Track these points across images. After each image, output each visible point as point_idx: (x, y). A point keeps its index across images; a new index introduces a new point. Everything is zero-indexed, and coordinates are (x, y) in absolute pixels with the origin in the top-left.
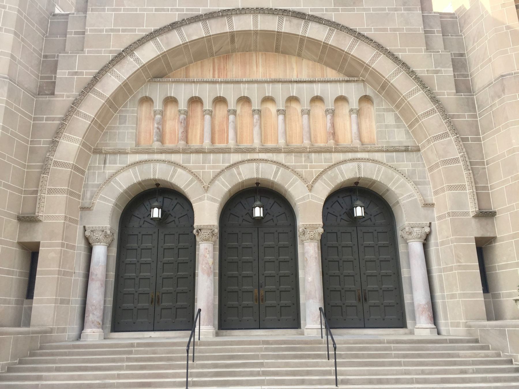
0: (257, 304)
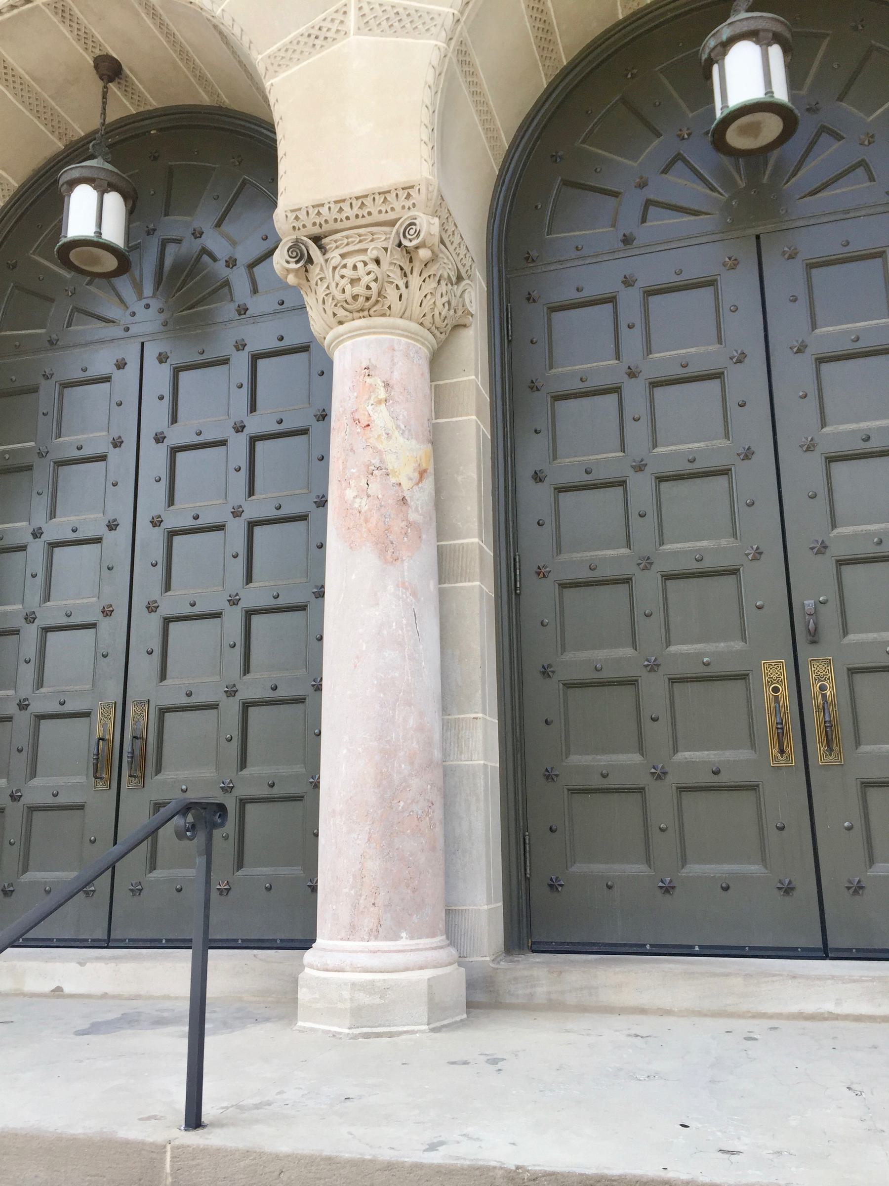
0: (795, 761)
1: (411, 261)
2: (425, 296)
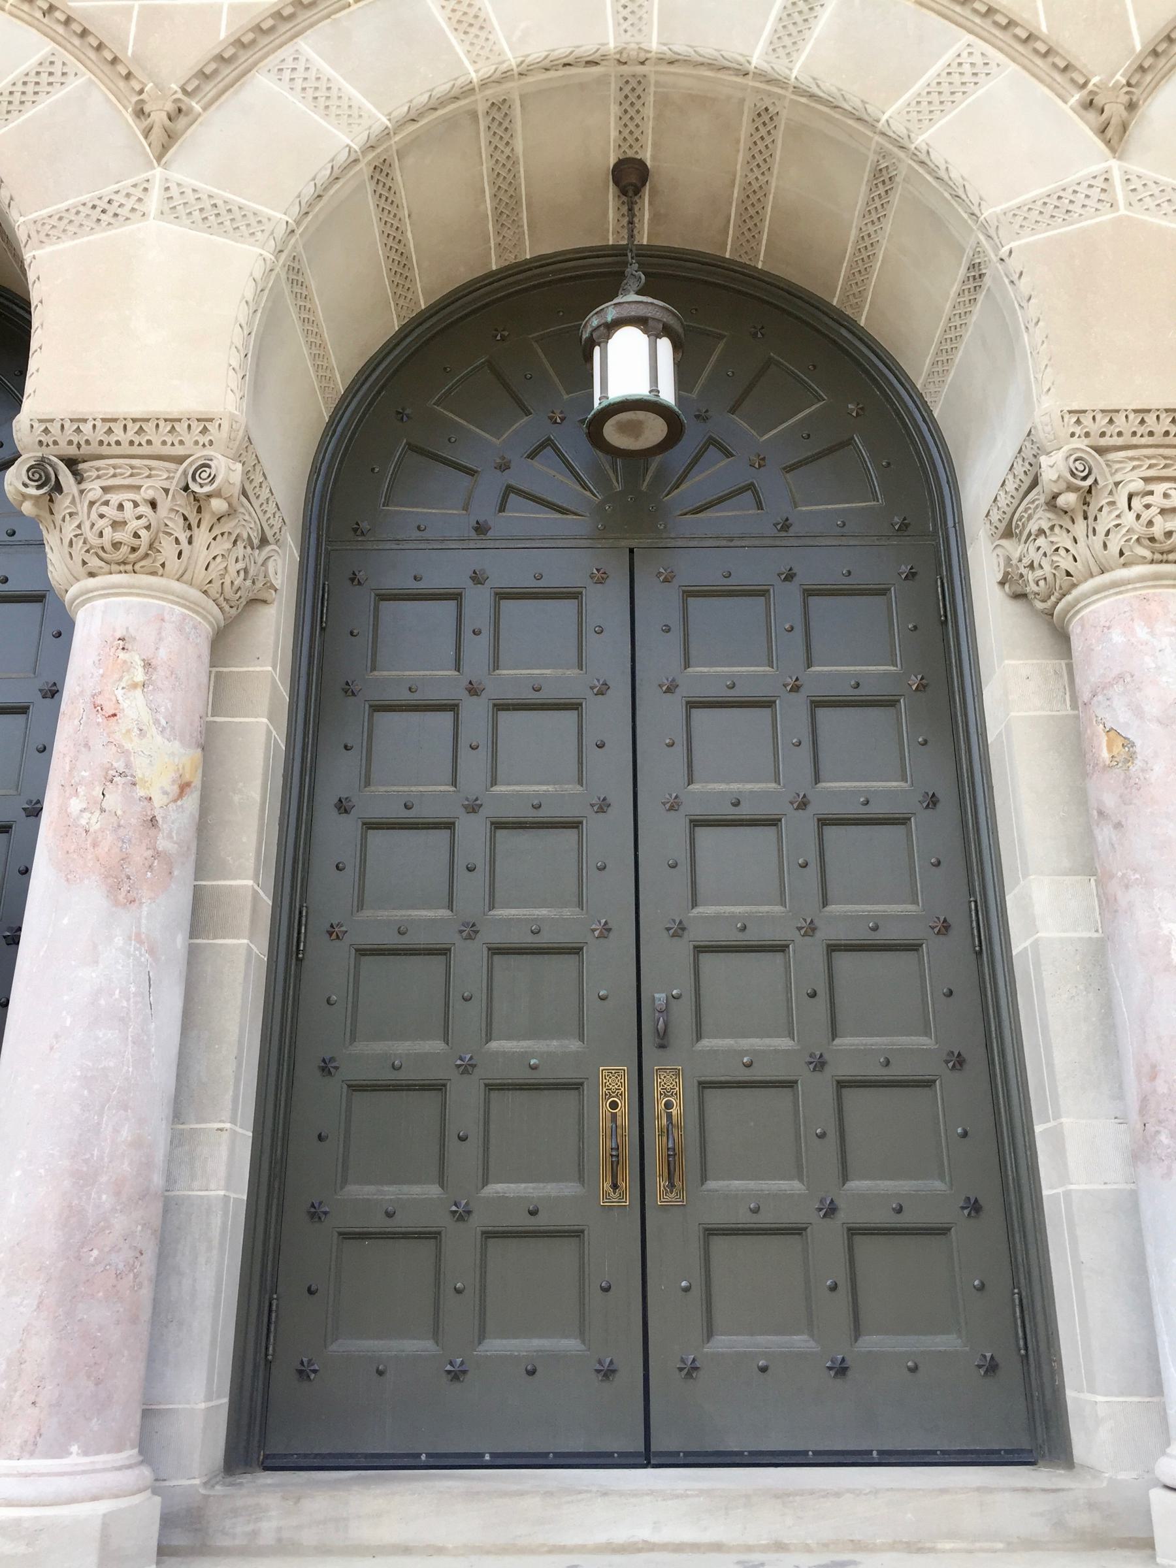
0: (629, 1200)
1: (199, 510)
2: (214, 558)
